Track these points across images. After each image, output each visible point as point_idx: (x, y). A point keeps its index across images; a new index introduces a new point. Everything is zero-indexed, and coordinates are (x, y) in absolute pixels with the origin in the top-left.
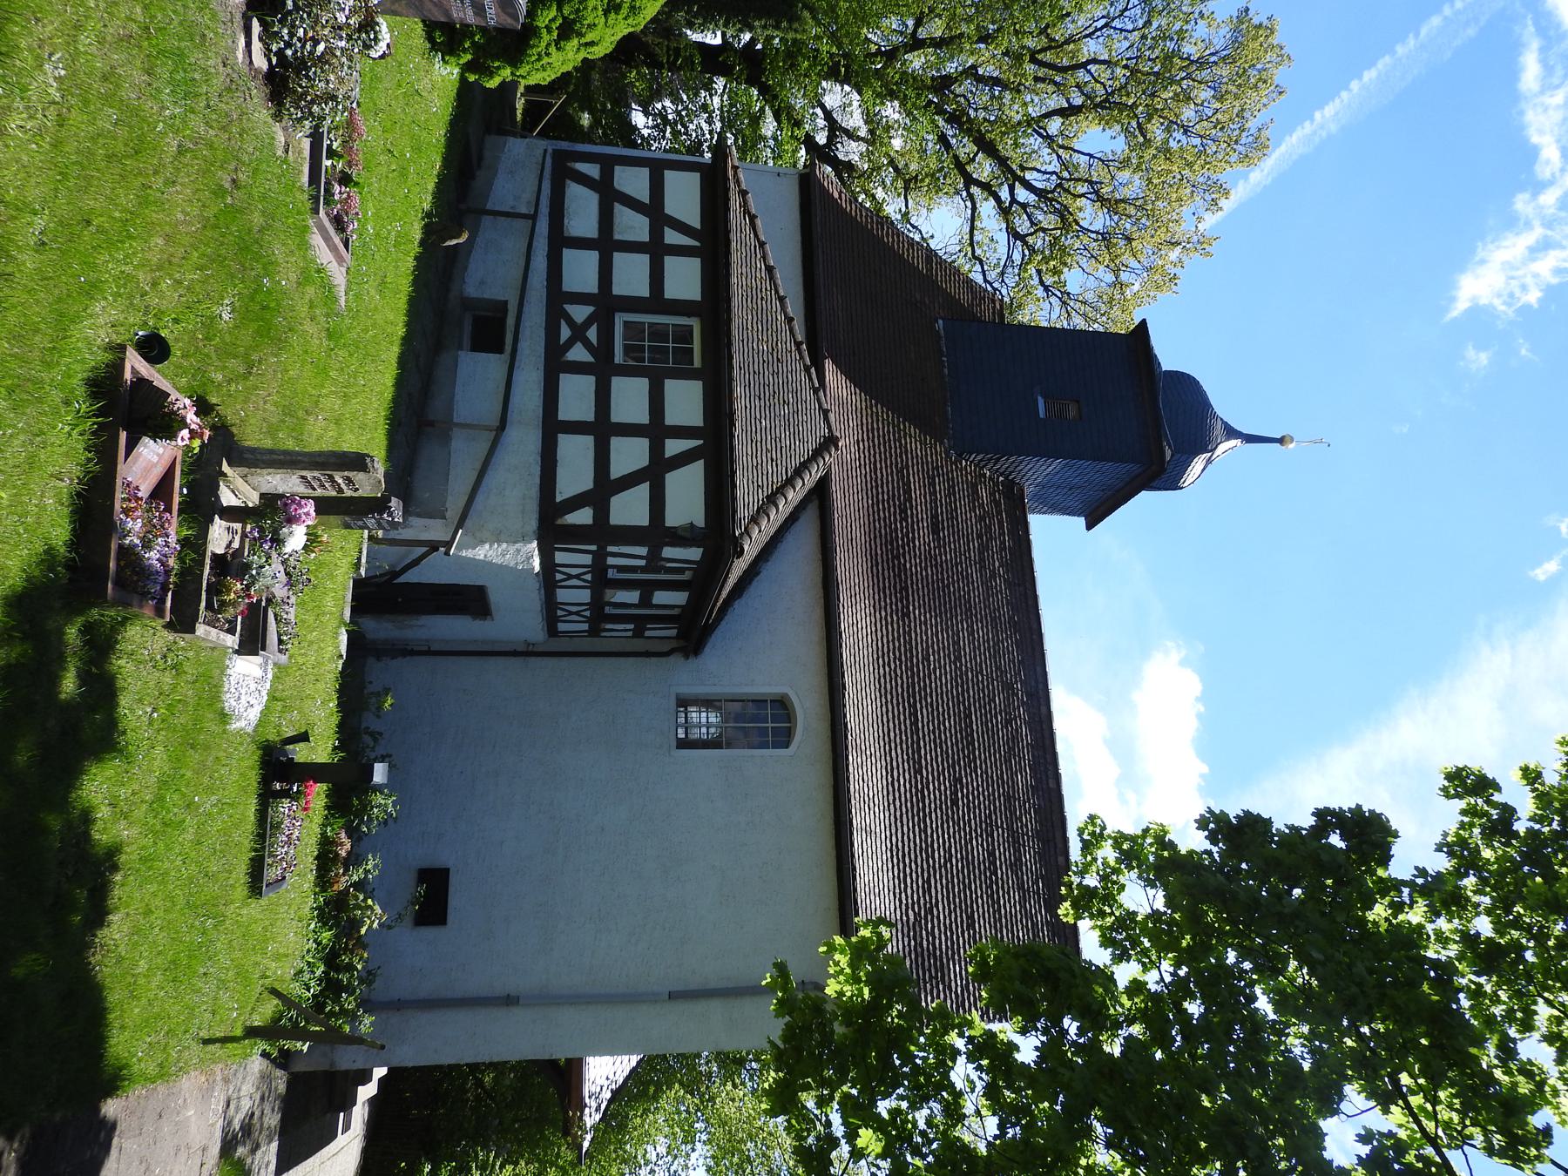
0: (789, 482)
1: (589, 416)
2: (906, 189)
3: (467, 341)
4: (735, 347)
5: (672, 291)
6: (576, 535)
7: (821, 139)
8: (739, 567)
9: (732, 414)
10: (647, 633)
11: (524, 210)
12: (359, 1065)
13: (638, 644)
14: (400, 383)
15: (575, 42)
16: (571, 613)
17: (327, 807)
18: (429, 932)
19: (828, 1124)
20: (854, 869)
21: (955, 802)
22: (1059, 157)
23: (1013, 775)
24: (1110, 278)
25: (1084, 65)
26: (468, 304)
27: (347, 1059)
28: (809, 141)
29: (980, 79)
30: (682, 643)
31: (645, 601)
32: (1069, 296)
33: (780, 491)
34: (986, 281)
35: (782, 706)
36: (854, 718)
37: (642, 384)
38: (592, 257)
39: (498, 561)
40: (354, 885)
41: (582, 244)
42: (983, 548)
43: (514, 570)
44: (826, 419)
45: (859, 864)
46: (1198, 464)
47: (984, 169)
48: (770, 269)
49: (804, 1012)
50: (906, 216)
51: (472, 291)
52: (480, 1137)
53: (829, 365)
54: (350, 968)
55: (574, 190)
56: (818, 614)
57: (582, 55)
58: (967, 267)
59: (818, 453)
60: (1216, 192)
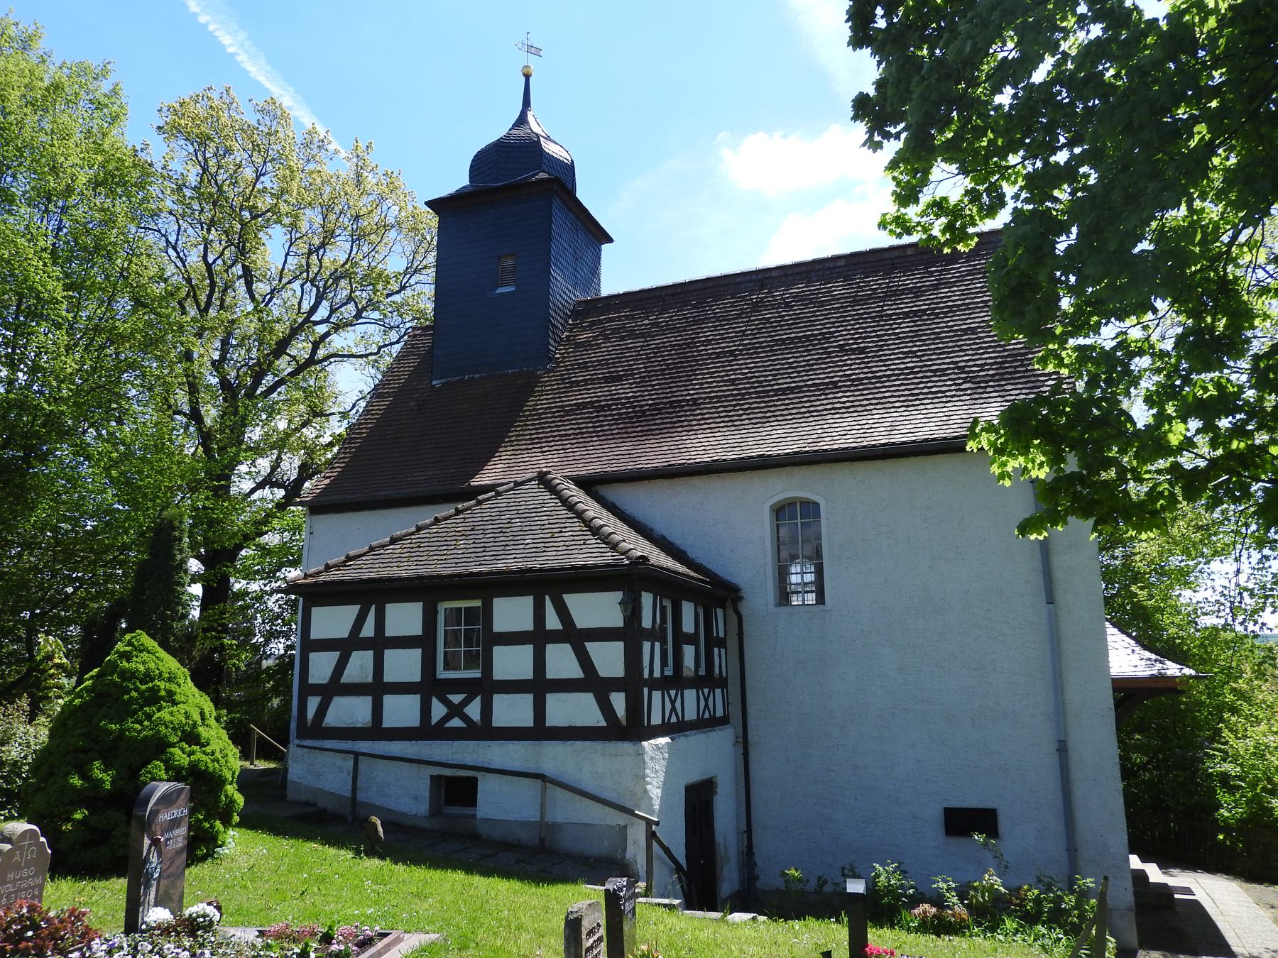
0: (580, 515)
2: (322, 414)
3: (468, 811)
4: (463, 570)
5: (416, 629)
6: (635, 707)
7: (280, 493)
8: (658, 558)
9: (521, 571)
10: (722, 635)
11: (351, 763)
12: (1129, 884)
13: (732, 642)
14: (507, 874)
15: (201, 729)
16: (706, 706)
17: (892, 927)
18: (1004, 824)
19: (1159, 472)
20: (926, 440)
21: (862, 351)
22: (290, 282)
23: (834, 298)
24: (392, 234)
25: (209, 267)
26: (435, 812)
27: (1123, 895)
28: (281, 506)
29: (223, 358)
30: (729, 603)
31: (692, 639)
32: (407, 265)
33: (587, 523)
34: (398, 342)
35: (782, 511)
36: (791, 447)
37: (498, 651)
39: (662, 776)
40: (961, 899)
42: (633, 335)
43: (669, 761)
44: (523, 483)
45: (921, 436)
46: (549, 148)
47: (300, 348)
48: (393, 541)
49: (1055, 501)
50: (344, 415)
51: (423, 808)
52: (1192, 765)
53: (476, 482)
54: (1038, 901)
55: (331, 719)
56: (697, 482)
57: (212, 722)
58: (387, 358)
59: (553, 490)
60: (313, 145)
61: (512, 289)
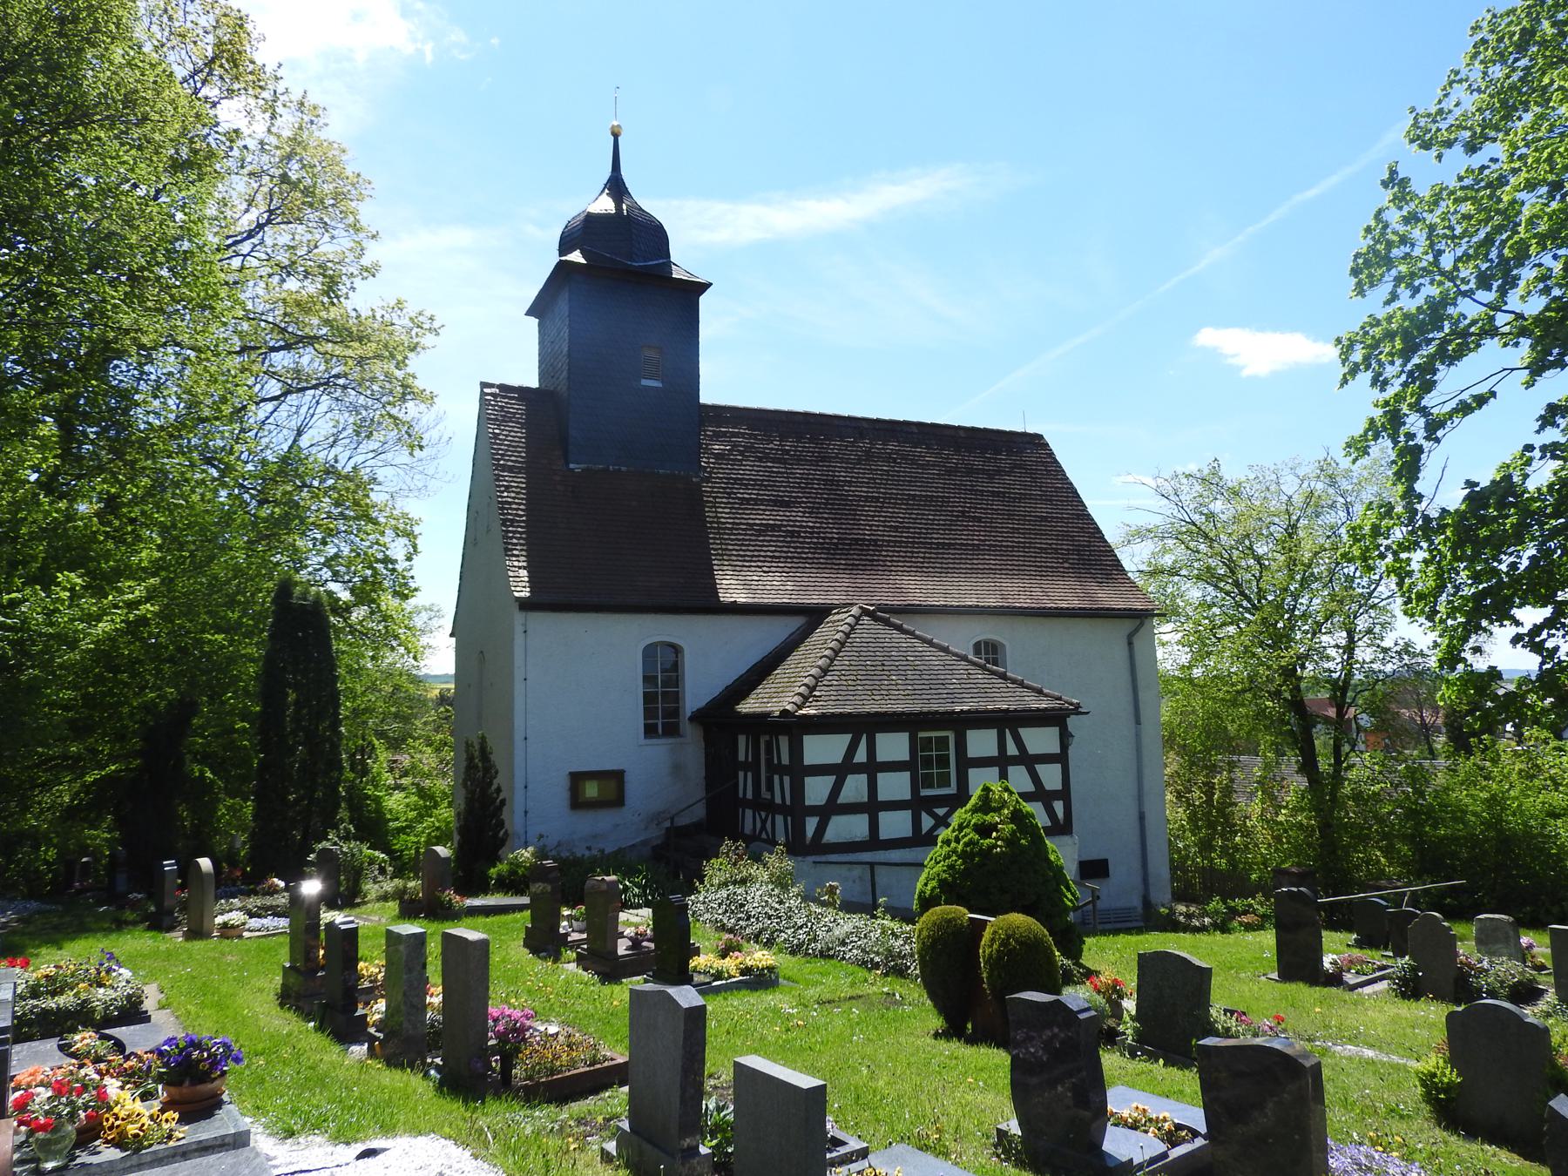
1: (865, 817)
21: (979, 520)
38: (884, 817)
41: (874, 826)
55: (830, 836)
61: (644, 382)
